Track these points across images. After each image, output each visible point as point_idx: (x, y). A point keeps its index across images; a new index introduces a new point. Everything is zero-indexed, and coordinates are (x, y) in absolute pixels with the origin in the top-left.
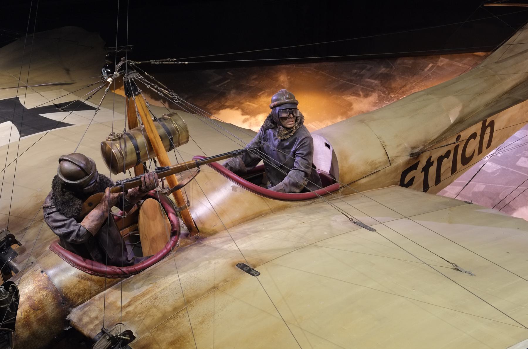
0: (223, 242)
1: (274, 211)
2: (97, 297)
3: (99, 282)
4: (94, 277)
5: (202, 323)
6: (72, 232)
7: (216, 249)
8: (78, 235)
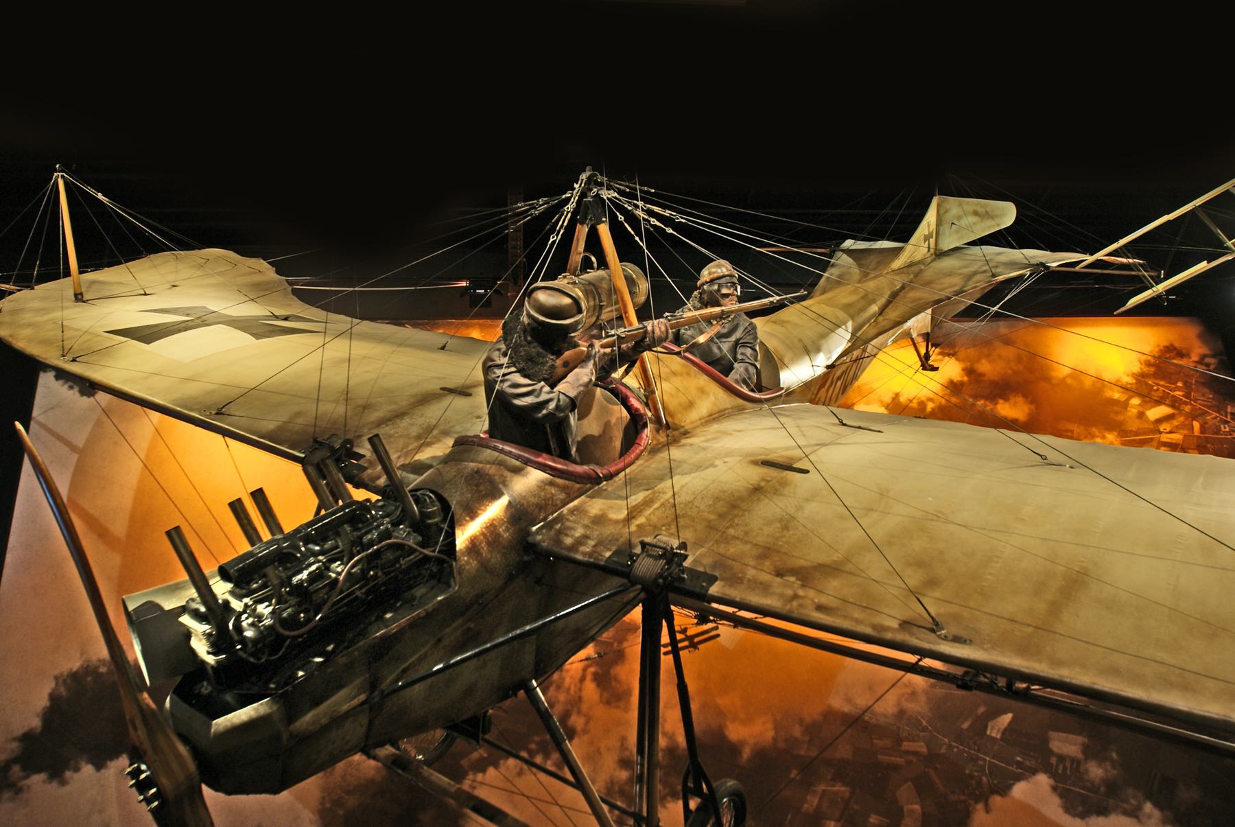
0: (708, 441)
1: (741, 410)
2: (565, 510)
3: (563, 488)
4: (559, 481)
5: (786, 528)
6: (548, 401)
7: (704, 449)
8: (557, 407)
